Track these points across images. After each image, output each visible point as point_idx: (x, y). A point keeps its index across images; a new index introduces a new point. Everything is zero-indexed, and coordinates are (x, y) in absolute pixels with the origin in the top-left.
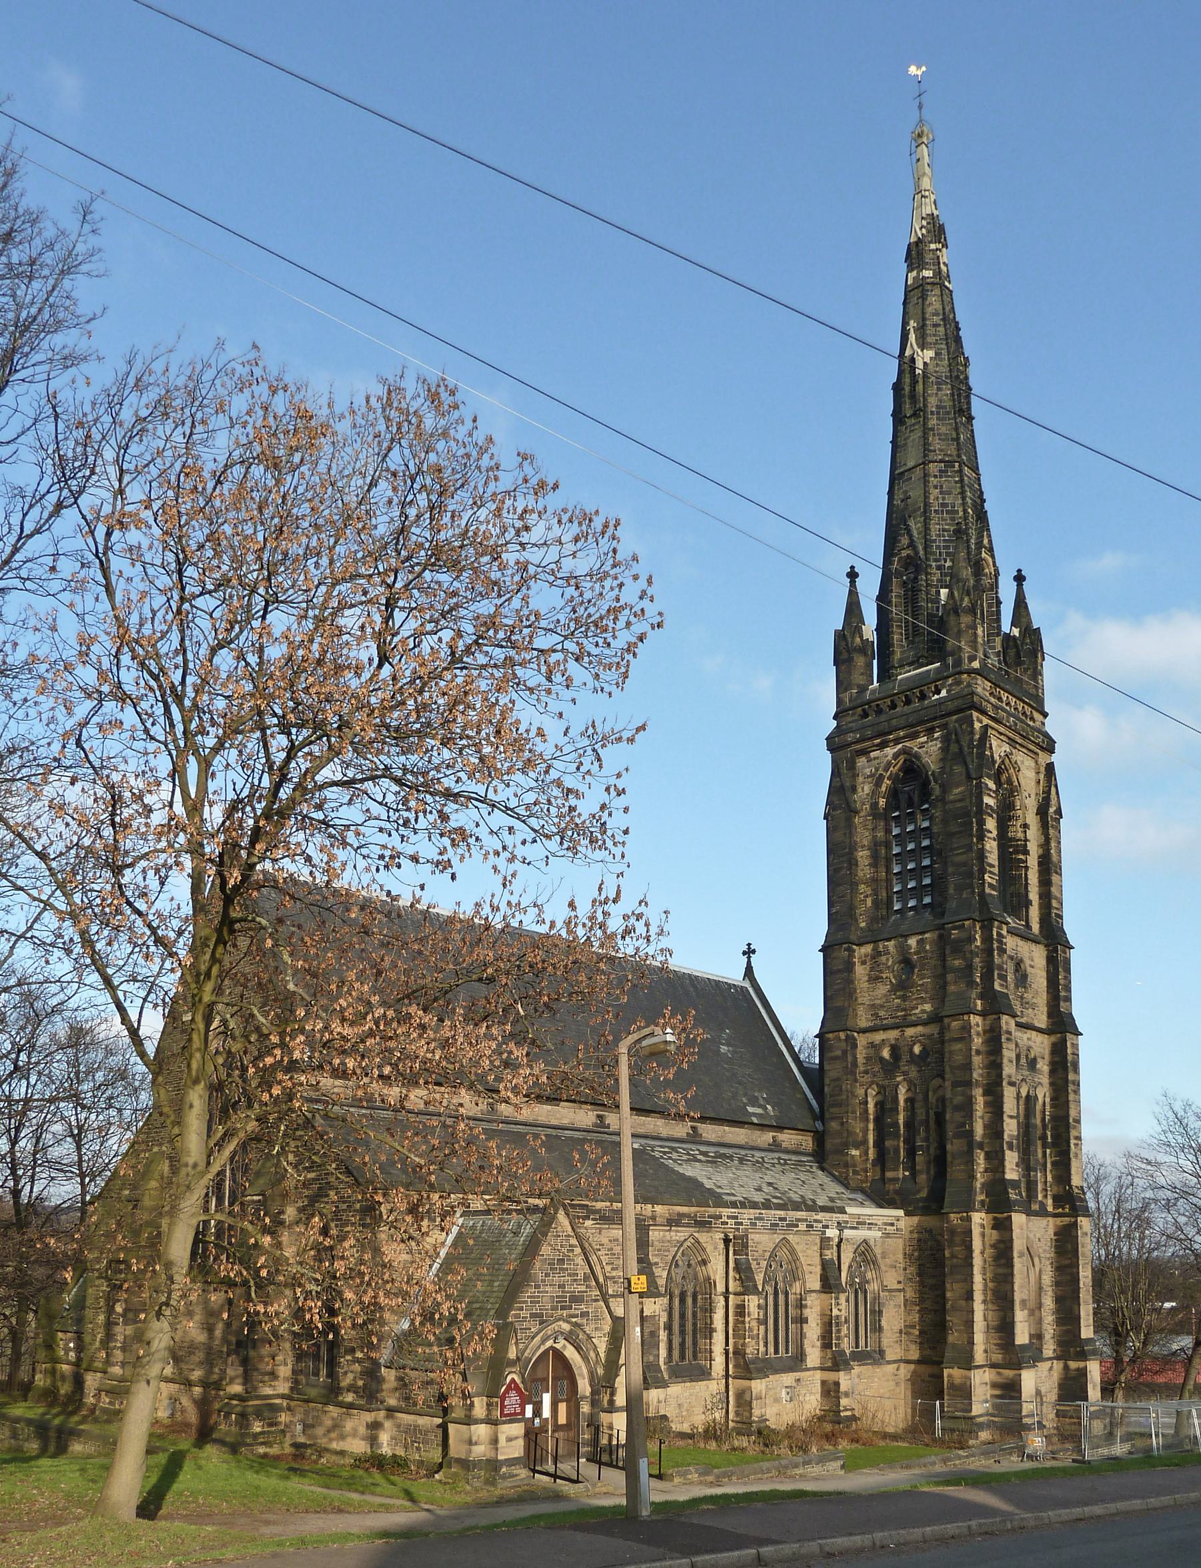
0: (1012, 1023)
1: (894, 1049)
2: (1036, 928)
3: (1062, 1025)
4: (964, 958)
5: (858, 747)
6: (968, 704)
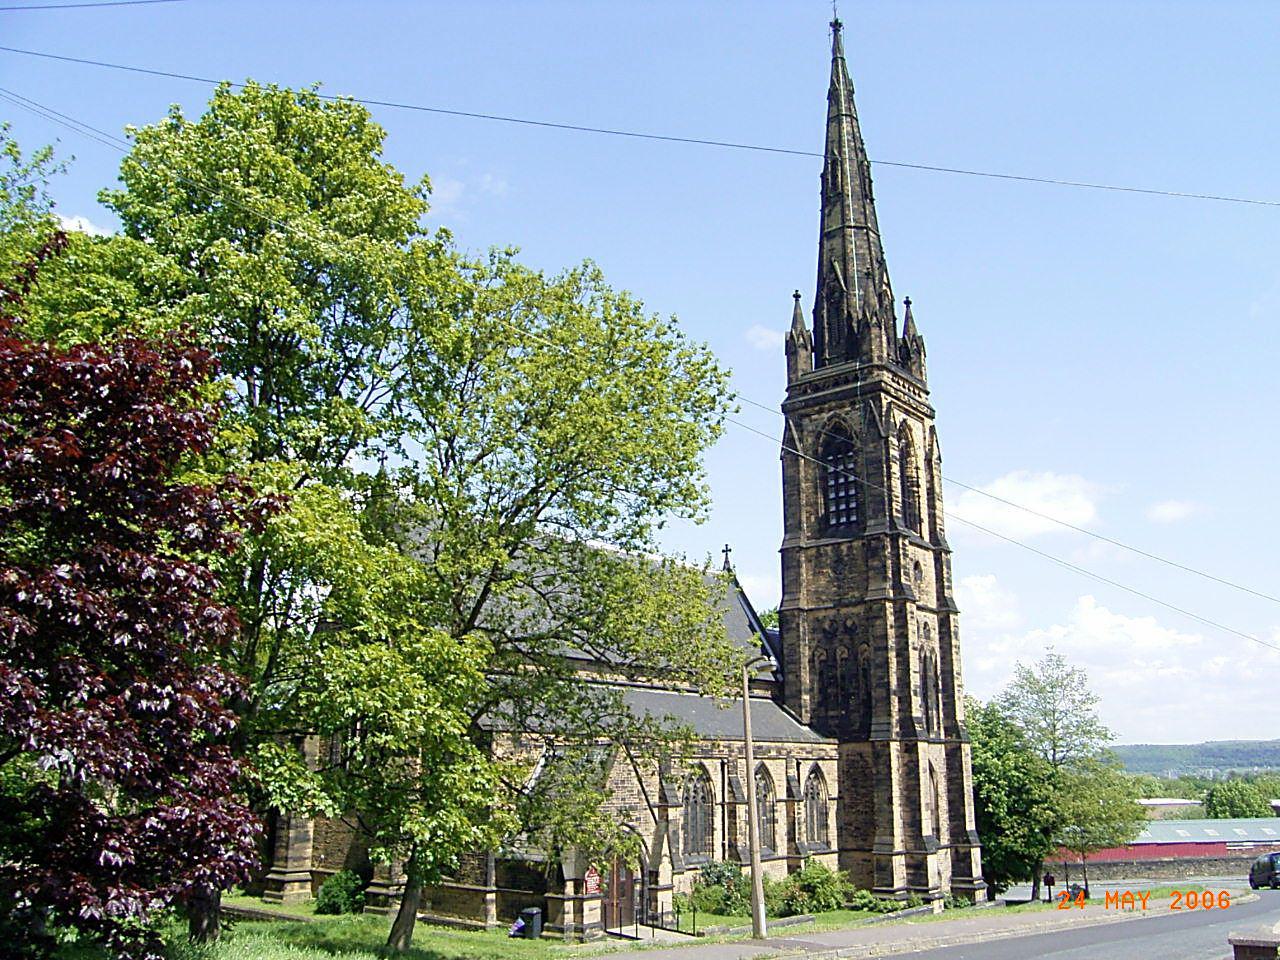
0: (914, 607)
1: (833, 621)
2: (927, 538)
3: (945, 609)
4: (880, 561)
5: (803, 411)
6: (877, 388)
